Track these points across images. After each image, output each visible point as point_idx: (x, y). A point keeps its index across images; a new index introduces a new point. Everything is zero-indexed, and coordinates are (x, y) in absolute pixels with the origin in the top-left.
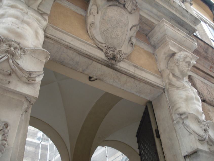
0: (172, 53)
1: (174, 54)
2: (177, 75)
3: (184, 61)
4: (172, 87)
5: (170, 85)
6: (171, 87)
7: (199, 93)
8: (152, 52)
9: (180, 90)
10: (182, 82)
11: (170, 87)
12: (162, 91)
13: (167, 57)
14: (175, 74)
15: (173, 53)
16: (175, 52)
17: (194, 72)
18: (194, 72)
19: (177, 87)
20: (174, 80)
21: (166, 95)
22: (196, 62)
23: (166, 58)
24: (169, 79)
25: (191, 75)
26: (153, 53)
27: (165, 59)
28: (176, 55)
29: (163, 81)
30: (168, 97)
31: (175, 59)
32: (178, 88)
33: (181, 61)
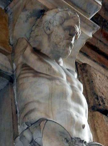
0: (39, 8)
1: (43, 12)
2: (44, 53)
3: (61, 24)
4: (27, 71)
5: (24, 68)
6: (24, 72)
7: (97, 96)
8: (3, 8)
9: (40, 77)
10: (47, 63)
11: (22, 72)
12: (6, 82)
13: (31, 17)
14: (42, 51)
15: (42, 9)
16: (45, 7)
17: (98, 61)
18: (98, 61)
19: (37, 72)
20: (32, 59)
21: (15, 88)
22: (93, 35)
23: (27, 19)
24: (24, 57)
25: (88, 63)
26: (5, 9)
27: (26, 21)
28: (47, 13)
29: (12, 62)
30: (17, 91)
31: (43, 22)
32: (37, 74)
33: (55, 24)
